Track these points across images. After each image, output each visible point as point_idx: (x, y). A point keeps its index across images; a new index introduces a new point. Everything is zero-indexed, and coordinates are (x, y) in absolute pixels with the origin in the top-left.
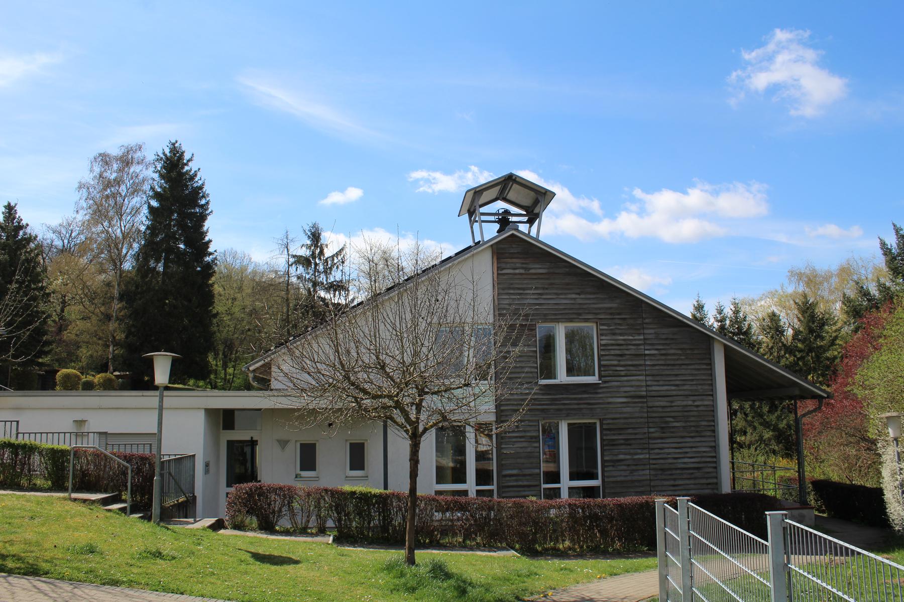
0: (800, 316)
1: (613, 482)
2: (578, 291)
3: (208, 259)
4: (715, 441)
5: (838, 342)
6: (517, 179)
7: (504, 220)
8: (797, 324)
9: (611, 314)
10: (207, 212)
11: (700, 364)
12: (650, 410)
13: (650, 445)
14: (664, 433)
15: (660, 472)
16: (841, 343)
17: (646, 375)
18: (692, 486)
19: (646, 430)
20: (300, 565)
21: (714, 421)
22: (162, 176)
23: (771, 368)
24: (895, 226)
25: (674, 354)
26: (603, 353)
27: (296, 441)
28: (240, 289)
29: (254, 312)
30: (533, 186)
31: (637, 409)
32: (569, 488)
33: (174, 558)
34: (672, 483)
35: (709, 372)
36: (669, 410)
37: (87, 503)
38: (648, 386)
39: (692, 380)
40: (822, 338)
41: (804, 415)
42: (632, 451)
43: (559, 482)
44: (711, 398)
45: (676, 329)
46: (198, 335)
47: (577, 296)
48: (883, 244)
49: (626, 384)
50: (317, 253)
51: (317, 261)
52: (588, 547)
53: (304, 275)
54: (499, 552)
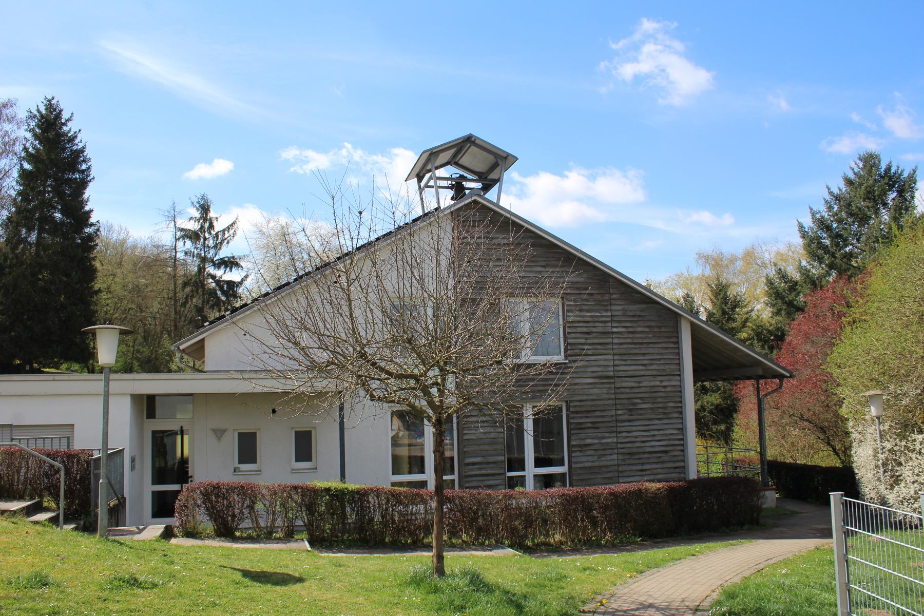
0: (712, 297)
1: (581, 468)
2: (543, 263)
3: (88, 230)
4: (682, 423)
5: (749, 324)
6: (477, 141)
7: (458, 188)
8: (709, 306)
9: (578, 289)
10: (89, 178)
11: (668, 342)
12: (618, 391)
13: (618, 428)
14: (631, 415)
15: (627, 457)
16: (751, 325)
17: (614, 355)
18: (660, 471)
19: (613, 413)
20: (306, 584)
21: (681, 402)
22: (36, 136)
23: (736, 347)
24: (811, 209)
25: (642, 332)
26: (569, 330)
27: (234, 430)
28: (120, 264)
29: (137, 289)
30: (493, 149)
31: (605, 391)
32: (535, 476)
33: (155, 585)
34: (640, 467)
35: (677, 351)
36: (636, 390)
37: (6, 514)
38: (616, 365)
39: (660, 359)
40: (734, 320)
41: (766, 395)
42: (600, 435)
43: (524, 470)
44: (678, 378)
45: (643, 306)
46: (78, 313)
47: (543, 269)
48: (801, 227)
49: (593, 363)
50: (206, 227)
51: (207, 235)
52: (580, 540)
53: (193, 251)
54: (495, 551)
